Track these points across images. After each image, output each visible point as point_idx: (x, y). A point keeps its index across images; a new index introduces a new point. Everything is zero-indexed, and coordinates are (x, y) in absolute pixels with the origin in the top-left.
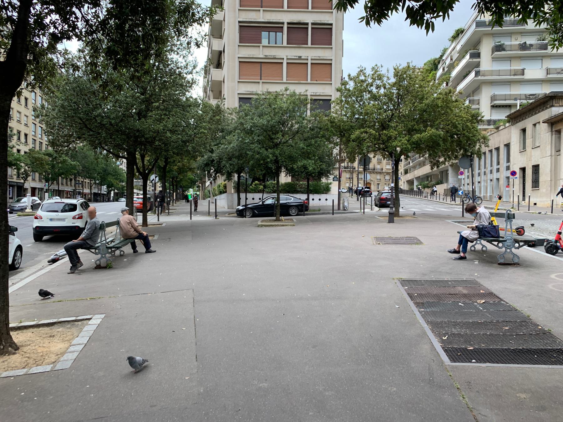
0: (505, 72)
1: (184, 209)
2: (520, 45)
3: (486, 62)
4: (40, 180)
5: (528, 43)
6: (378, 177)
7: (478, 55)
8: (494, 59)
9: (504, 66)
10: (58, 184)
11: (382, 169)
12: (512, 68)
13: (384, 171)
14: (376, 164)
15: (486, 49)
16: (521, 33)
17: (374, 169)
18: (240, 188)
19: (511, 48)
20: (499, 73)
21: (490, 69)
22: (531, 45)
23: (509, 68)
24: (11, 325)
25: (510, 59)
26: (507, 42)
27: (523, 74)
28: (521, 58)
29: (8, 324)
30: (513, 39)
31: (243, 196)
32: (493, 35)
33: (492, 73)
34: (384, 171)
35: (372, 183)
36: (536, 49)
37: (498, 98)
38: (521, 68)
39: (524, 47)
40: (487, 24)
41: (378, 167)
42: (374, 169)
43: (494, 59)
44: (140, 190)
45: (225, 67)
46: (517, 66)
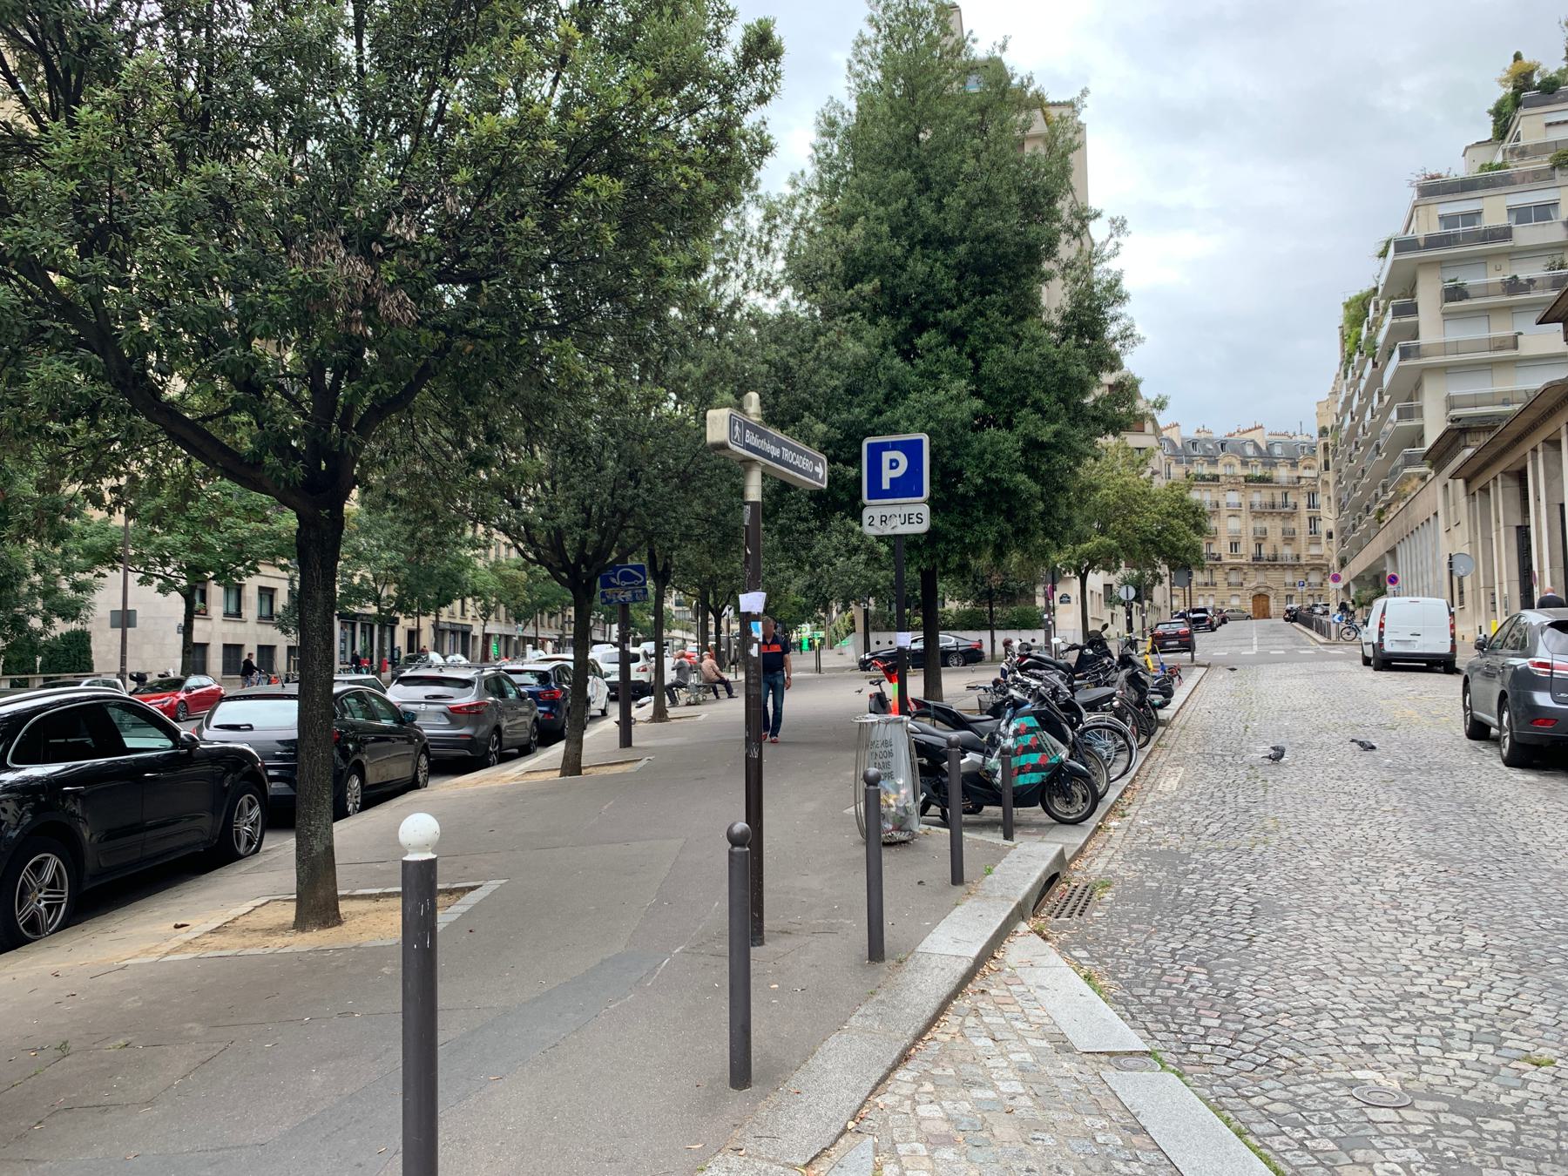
0: (1474, 346)
1: (1498, 530)
2: (1503, 282)
3: (1432, 328)
4: (508, 622)
5: (1523, 276)
6: (1289, 577)
7: (1413, 309)
8: (1448, 316)
9: (1477, 332)
10: (535, 625)
11: (1298, 557)
12: (1494, 334)
13: (1303, 561)
14: (1280, 544)
15: (1428, 295)
16: (1509, 254)
17: (1275, 559)
18: (871, 624)
19: (1487, 290)
20: (1456, 348)
21: (1441, 339)
22: (1531, 281)
23: (1486, 335)
24: (439, 886)
25: (1487, 312)
26: (1471, 279)
27: (1516, 347)
28: (1510, 309)
29: (433, 883)
30: (1491, 268)
31: (873, 637)
32: (1441, 263)
33: (1444, 348)
34: (1303, 561)
35: (1271, 594)
36: (1544, 288)
37: (1457, 402)
38: (1511, 333)
39: (1513, 286)
40: (1422, 243)
41: (1287, 551)
42: (1275, 559)
43: (1448, 316)
44: (688, 630)
45: (260, 628)
46: (1501, 329)
